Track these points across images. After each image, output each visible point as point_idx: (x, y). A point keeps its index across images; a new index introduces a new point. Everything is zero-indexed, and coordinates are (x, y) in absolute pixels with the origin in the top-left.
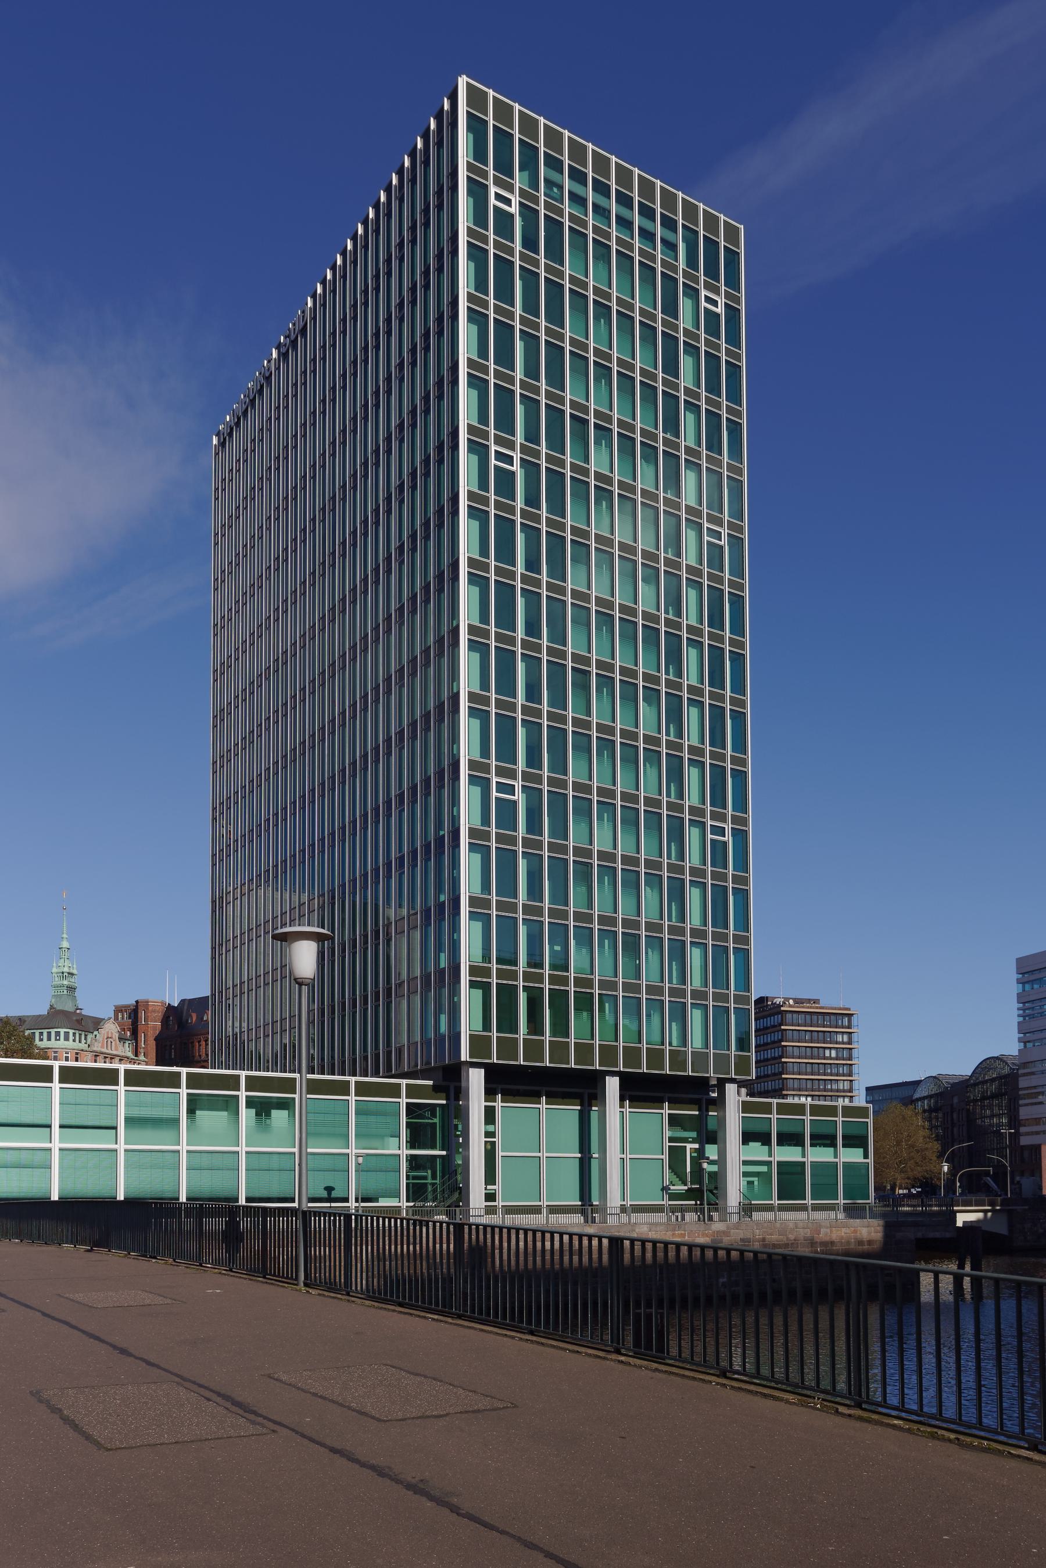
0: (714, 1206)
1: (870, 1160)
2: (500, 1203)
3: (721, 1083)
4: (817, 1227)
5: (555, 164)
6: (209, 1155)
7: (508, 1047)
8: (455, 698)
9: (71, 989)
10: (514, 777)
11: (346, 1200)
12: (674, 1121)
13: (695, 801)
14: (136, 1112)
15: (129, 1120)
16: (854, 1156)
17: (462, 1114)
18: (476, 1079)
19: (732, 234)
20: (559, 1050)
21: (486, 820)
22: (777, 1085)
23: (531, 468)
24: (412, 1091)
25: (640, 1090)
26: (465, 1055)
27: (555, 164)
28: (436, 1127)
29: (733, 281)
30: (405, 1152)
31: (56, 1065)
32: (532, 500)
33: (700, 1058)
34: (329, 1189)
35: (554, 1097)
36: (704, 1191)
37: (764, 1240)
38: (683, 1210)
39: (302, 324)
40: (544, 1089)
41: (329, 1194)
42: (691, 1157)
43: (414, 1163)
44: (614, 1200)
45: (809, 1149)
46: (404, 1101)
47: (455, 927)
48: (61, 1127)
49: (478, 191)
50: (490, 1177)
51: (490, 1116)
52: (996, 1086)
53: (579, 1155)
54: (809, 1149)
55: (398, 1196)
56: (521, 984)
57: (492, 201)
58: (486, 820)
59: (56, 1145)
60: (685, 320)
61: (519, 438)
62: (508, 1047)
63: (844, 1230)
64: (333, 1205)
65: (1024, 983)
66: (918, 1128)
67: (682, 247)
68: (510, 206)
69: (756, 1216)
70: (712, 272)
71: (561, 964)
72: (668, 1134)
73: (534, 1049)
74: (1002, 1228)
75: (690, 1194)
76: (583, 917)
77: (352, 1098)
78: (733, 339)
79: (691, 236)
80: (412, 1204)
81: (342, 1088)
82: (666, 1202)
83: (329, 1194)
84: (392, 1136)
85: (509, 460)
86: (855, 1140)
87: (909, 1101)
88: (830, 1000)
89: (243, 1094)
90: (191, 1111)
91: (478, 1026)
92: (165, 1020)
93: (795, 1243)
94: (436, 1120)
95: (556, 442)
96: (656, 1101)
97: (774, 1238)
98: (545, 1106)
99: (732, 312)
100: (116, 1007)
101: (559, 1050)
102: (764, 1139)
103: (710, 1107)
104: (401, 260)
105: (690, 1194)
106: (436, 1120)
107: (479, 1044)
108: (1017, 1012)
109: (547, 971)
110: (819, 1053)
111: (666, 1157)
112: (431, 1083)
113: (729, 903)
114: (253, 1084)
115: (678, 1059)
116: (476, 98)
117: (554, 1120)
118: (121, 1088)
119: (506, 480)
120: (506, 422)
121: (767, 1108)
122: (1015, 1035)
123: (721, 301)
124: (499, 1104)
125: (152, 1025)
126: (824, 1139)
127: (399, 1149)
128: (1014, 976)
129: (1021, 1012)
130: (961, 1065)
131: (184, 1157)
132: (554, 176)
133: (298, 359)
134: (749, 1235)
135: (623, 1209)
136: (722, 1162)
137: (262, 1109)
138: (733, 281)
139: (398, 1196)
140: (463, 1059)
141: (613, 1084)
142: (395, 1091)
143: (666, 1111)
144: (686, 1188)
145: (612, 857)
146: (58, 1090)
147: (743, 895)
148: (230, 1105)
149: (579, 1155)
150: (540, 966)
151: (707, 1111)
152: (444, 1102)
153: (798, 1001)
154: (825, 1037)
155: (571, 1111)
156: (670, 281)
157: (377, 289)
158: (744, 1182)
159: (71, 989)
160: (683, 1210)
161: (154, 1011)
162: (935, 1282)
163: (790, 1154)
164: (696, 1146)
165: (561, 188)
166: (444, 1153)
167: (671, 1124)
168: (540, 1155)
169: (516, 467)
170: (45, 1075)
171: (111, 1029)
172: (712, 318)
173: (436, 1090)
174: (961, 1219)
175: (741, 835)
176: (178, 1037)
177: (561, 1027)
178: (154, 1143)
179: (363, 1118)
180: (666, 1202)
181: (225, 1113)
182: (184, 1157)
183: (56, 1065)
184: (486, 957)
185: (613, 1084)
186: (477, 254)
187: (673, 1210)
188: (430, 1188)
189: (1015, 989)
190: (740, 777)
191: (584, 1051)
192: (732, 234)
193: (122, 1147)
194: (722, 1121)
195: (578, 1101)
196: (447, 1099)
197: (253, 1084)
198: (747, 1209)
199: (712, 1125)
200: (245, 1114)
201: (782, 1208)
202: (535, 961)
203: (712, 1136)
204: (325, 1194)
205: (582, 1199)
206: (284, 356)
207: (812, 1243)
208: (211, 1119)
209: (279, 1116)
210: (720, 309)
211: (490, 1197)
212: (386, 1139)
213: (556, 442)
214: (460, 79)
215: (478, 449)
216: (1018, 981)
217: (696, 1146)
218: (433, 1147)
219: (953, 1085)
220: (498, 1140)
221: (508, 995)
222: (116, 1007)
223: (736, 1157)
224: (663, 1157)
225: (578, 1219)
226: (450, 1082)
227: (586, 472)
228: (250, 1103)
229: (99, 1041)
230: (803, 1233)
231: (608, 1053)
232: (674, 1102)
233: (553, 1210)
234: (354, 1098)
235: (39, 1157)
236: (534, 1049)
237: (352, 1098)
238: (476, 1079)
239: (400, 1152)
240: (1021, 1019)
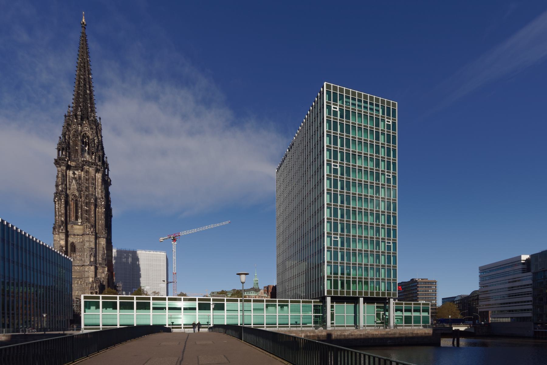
1: (430, 315)
2: (335, 325)
3: (389, 299)
4: (414, 330)
5: (348, 97)
7: (336, 292)
8: (324, 219)
9: (257, 283)
10: (337, 235)
12: (377, 307)
13: (383, 236)
14: (255, 307)
15: (254, 309)
16: (426, 314)
17: (326, 306)
18: (329, 299)
20: (348, 293)
21: (331, 245)
22: (416, 298)
23: (342, 167)
25: (368, 300)
26: (326, 294)
27: (348, 97)
28: (320, 309)
29: (394, 116)
30: (313, 315)
31: (252, 299)
32: (342, 174)
33: (383, 294)
34: (296, 322)
35: (347, 303)
36: (385, 322)
38: (380, 326)
43: (316, 317)
44: (362, 324)
45: (422, 313)
46: (313, 304)
47: (324, 268)
49: (329, 107)
50: (332, 319)
51: (332, 307)
52: (474, 298)
54: (422, 313)
56: (339, 279)
58: (331, 245)
60: (381, 127)
61: (339, 161)
62: (336, 292)
66: (455, 308)
67: (381, 111)
69: (398, 327)
70: (388, 114)
71: (349, 274)
72: (376, 310)
73: (342, 293)
74: (473, 331)
75: (382, 323)
78: (394, 129)
79: (383, 108)
81: (299, 302)
82: (376, 325)
85: (337, 166)
87: (454, 302)
88: (430, 279)
89: (277, 304)
90: (267, 307)
91: (329, 288)
92: (272, 289)
93: (408, 333)
95: (348, 160)
96: (373, 303)
97: (402, 333)
99: (394, 124)
101: (348, 293)
102: (401, 311)
105: (382, 323)
107: (329, 292)
109: (345, 276)
110: (427, 291)
111: (375, 315)
113: (391, 258)
114: (279, 301)
115: (378, 294)
116: (328, 87)
117: (347, 308)
118: (252, 303)
119: (336, 171)
120: (336, 158)
121: (402, 304)
122: (478, 285)
123: (391, 121)
124: (335, 304)
125: (270, 290)
127: (312, 314)
128: (478, 271)
130: (468, 293)
131: (197, 316)
132: (348, 100)
133: (292, 150)
135: (364, 326)
136: (389, 315)
137: (282, 306)
141: (361, 300)
142: (311, 302)
143: (376, 305)
145: (361, 251)
147: (395, 257)
148: (275, 306)
150: (337, 274)
153: (422, 279)
154: (429, 287)
155: (352, 306)
156: (377, 119)
158: (395, 320)
159: (257, 283)
160: (380, 326)
162: (446, 342)
163: (408, 314)
165: (349, 103)
169: (338, 167)
170: (250, 301)
171: (262, 291)
172: (388, 126)
174: (454, 328)
175: (395, 244)
176: (273, 292)
177: (349, 288)
178: (259, 313)
179: (262, 308)
180: (376, 325)
182: (197, 316)
183: (252, 299)
184: (331, 273)
185: (361, 300)
186: (329, 121)
187: (377, 326)
189: (478, 274)
190: (395, 230)
191: (354, 293)
192: (394, 105)
193: (252, 314)
194: (389, 307)
198: (396, 326)
199: (387, 308)
201: (405, 326)
202: (342, 274)
203: (388, 310)
206: (289, 150)
207: (412, 333)
209: (285, 308)
210: (391, 123)
211: (332, 324)
213: (348, 160)
215: (329, 165)
219: (465, 297)
220: (334, 312)
221: (336, 282)
223: (393, 315)
225: (354, 328)
227: (355, 166)
228: (279, 305)
229: (260, 293)
230: (410, 332)
231: (360, 293)
232: (377, 303)
233: (347, 326)
235: (286, 317)
236: (342, 293)
237: (301, 304)
238: (329, 299)
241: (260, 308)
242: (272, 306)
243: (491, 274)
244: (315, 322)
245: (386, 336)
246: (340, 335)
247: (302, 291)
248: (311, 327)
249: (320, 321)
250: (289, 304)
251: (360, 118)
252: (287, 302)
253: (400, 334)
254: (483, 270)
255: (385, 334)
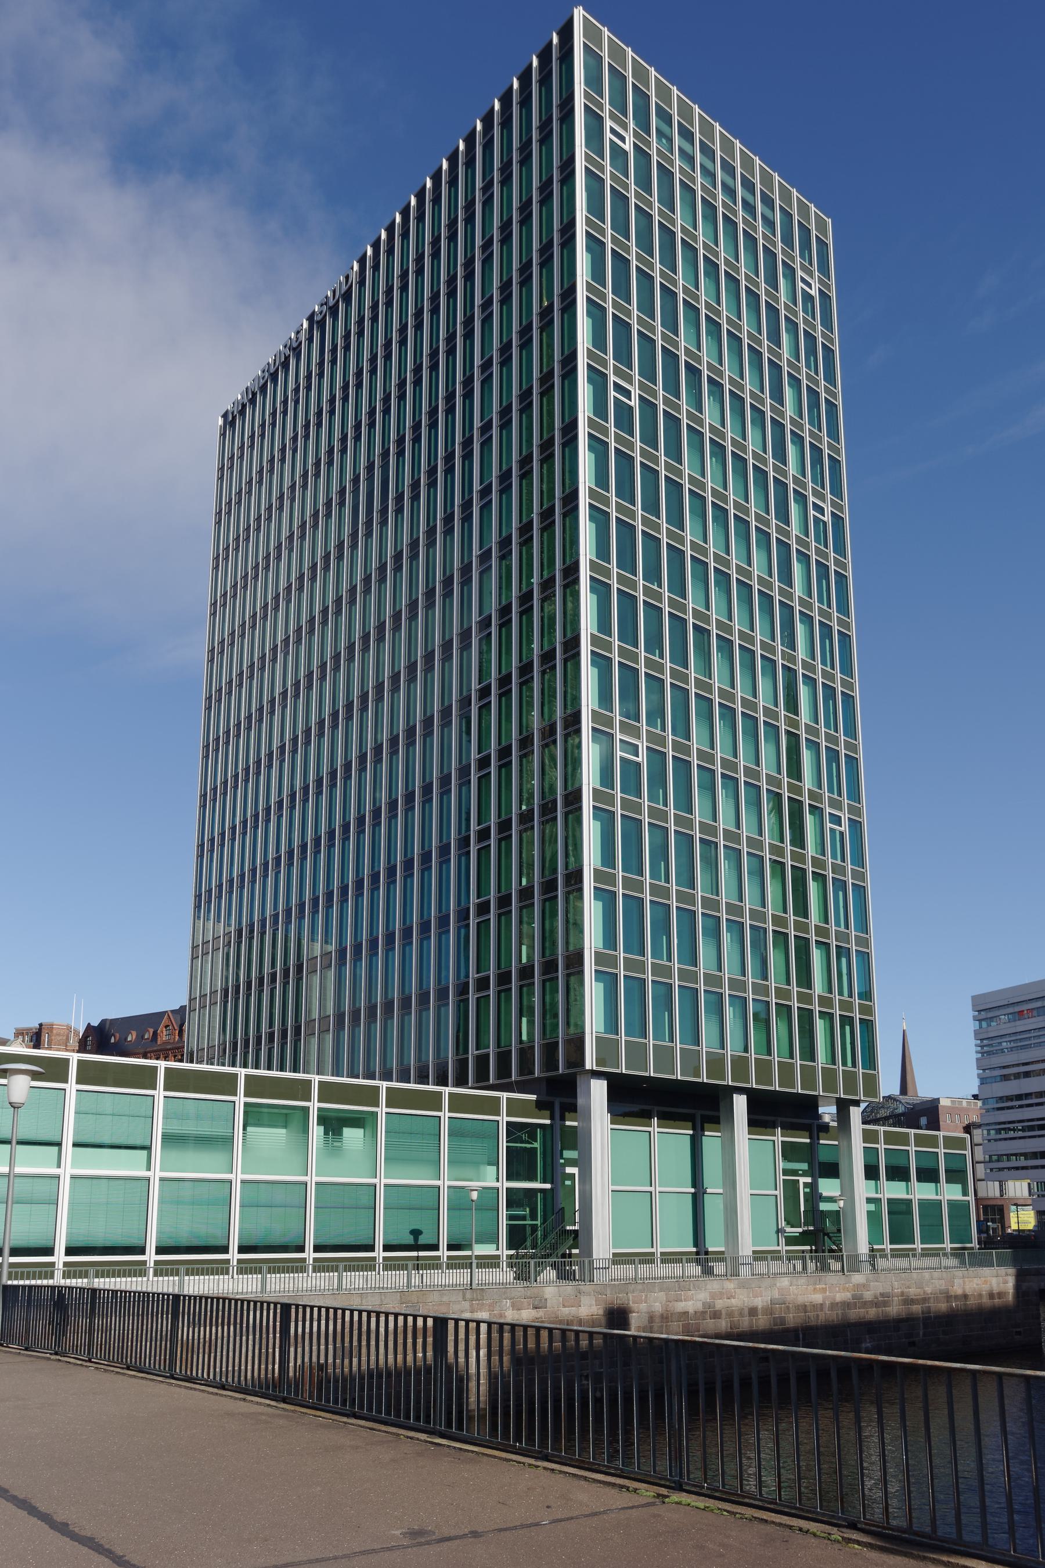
0: (836, 1254)
6: (89, 1181)
11: (435, 1247)
14: (177, 1128)
15: (168, 1139)
16: (951, 1192)
19: (821, 226)
20: (691, 1059)
24: (514, 1107)
25: (768, 1111)
34: (416, 1233)
35: (668, 1118)
36: (818, 1234)
37: (902, 1294)
39: (344, 288)
40: (656, 1108)
41: (416, 1239)
42: (805, 1193)
43: (514, 1198)
46: (504, 1119)
48: (75, 1145)
53: (693, 1190)
55: (496, 1241)
57: (608, 135)
59: (67, 1170)
63: (975, 1280)
64: (422, 1254)
65: (980, 1021)
68: (624, 143)
72: (781, 1165)
75: (803, 1238)
76: (711, 904)
77: (445, 1114)
79: (787, 215)
80: (512, 1252)
83: (416, 1239)
84: (489, 1164)
86: (956, 1175)
94: (536, 1145)
98: (657, 1130)
100: (17, 1030)
102: (897, 1173)
103: (821, 1134)
104: (297, 402)
105: (803, 1238)
106: (536, 1145)
108: (974, 1049)
111: (780, 1192)
112: (534, 1097)
114: (328, 1092)
118: (72, 1086)
126: (928, 1175)
127: (494, 1178)
128: (970, 1013)
129: (979, 1049)
134: (888, 1290)
137: (333, 1124)
138: (824, 268)
139: (496, 1241)
140: (588, 1066)
141: (740, 1103)
142: (493, 1107)
143: (779, 1137)
144: (800, 1230)
146: (74, 1093)
149: (693, 1190)
151: (563, 1119)
152: (548, 1122)
155: (679, 1138)
157: (274, 424)
161: (58, 1035)
164: (809, 1180)
166: (548, 1186)
167: (785, 1157)
168: (652, 1189)
173: (541, 1106)
175: (856, 825)
179: (218, 1129)
180: (783, 1248)
181: (284, 1131)
185: (740, 1103)
188: (528, 1230)
189: (971, 1026)
191: (716, 1064)
192: (821, 226)
195: (690, 1124)
196: (552, 1118)
197: (328, 1092)
200: (316, 1131)
204: (409, 1240)
205: (696, 1245)
207: (949, 1297)
208: (273, 1138)
209: (352, 1135)
212: (482, 1167)
214: (576, 11)
216: (975, 1019)
217: (809, 1180)
218: (532, 1178)
222: (17, 1030)
224: (777, 1193)
226: (560, 1093)
228: (324, 1119)
231: (740, 1065)
232: (789, 1127)
234: (448, 1114)
235: (42, 1189)
239: (499, 1185)
240: (980, 1055)
241: (205, 1129)
242: (282, 1118)
243: (1022, 1025)
244: (516, 1237)
245: (854, 1314)
246: (666, 1318)
247: (437, 1032)
248: (491, 1262)
249: (546, 1231)
250: (382, 1110)
251: (92, 1271)
252: (370, 1096)
253: (908, 1301)
254: (987, 1010)
255: (846, 1305)
